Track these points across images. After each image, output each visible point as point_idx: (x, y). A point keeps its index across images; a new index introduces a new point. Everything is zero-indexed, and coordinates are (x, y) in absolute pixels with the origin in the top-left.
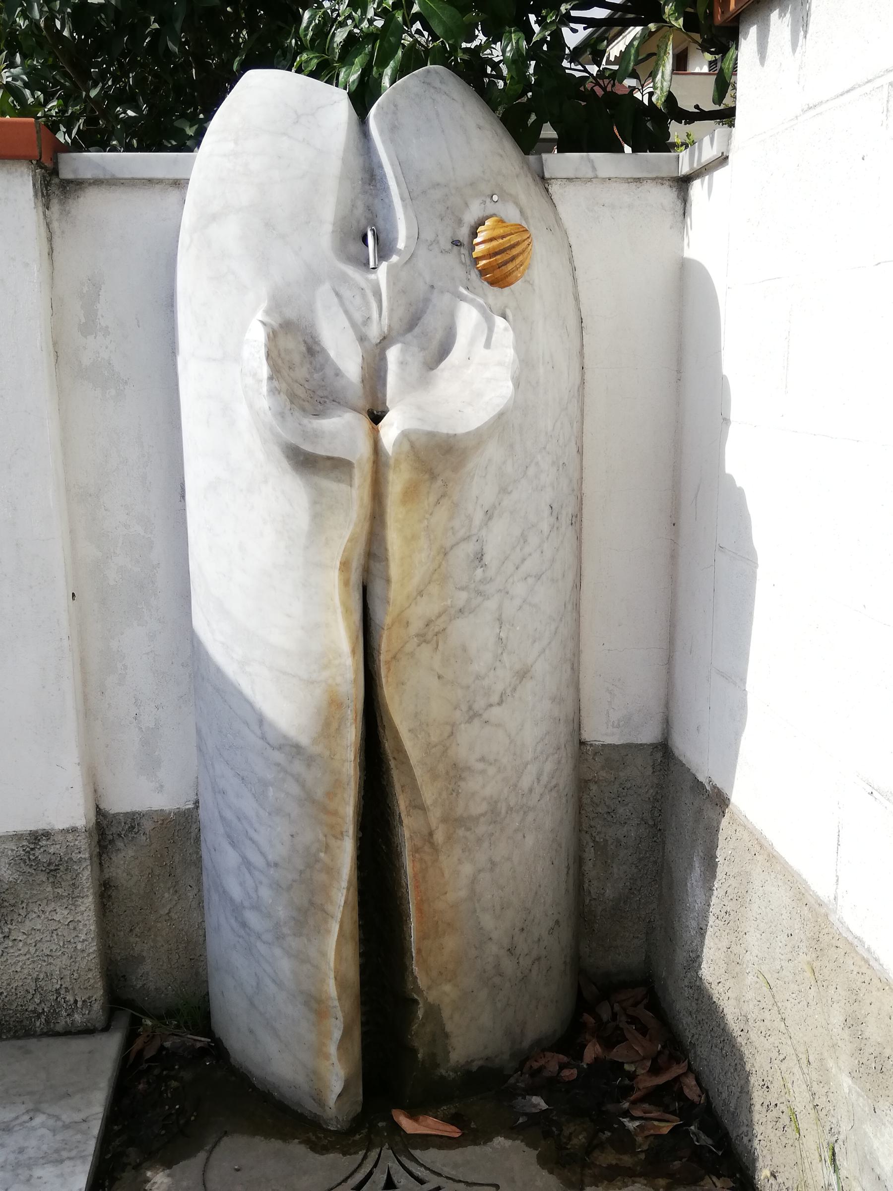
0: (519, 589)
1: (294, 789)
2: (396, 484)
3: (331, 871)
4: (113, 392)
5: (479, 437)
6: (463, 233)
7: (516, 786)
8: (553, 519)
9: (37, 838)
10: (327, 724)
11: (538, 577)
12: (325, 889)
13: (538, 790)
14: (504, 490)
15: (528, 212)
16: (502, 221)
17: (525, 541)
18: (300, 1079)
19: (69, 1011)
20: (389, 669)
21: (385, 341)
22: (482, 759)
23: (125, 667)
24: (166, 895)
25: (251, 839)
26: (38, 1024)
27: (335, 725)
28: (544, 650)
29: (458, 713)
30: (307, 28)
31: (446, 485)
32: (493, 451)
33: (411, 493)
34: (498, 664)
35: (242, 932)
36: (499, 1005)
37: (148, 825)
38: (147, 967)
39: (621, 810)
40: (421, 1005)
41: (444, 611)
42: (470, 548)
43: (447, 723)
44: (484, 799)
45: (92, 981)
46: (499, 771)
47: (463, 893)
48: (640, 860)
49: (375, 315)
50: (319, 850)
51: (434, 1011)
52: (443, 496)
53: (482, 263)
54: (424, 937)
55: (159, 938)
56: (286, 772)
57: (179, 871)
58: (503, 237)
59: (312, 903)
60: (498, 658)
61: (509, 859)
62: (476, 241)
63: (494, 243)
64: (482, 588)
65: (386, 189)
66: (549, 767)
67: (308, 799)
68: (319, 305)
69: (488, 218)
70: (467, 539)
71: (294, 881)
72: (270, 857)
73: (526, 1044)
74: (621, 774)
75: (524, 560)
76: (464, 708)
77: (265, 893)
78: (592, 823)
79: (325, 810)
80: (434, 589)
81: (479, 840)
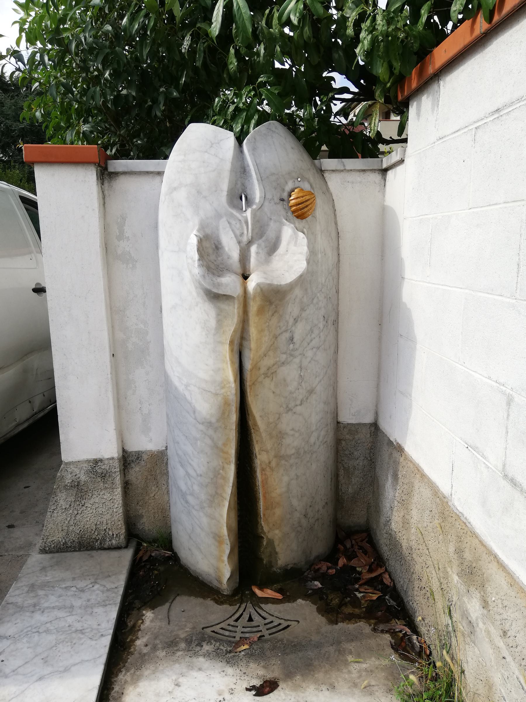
0: (310, 354)
1: (208, 441)
2: (253, 308)
3: (224, 478)
4: (131, 265)
5: (292, 286)
6: (285, 195)
7: (308, 442)
9: (97, 462)
10: (223, 413)
14: (303, 309)
15: (314, 186)
16: (302, 190)
18: (211, 571)
21: (250, 243)
22: (293, 429)
24: (153, 488)
25: (190, 464)
26: (97, 544)
28: (320, 381)
29: (282, 409)
30: (217, 106)
31: (276, 307)
32: (298, 292)
33: (261, 311)
34: (300, 387)
37: (145, 457)
38: (144, 520)
39: (356, 453)
42: (287, 335)
45: (120, 526)
49: (245, 232)
51: (271, 542)
52: (275, 312)
54: (266, 508)
58: (302, 197)
59: (217, 493)
60: (300, 384)
64: (292, 353)
65: (251, 176)
66: (323, 433)
67: (215, 446)
69: (296, 188)
70: (286, 331)
74: (356, 437)
75: (311, 340)
76: (285, 406)
80: (271, 353)
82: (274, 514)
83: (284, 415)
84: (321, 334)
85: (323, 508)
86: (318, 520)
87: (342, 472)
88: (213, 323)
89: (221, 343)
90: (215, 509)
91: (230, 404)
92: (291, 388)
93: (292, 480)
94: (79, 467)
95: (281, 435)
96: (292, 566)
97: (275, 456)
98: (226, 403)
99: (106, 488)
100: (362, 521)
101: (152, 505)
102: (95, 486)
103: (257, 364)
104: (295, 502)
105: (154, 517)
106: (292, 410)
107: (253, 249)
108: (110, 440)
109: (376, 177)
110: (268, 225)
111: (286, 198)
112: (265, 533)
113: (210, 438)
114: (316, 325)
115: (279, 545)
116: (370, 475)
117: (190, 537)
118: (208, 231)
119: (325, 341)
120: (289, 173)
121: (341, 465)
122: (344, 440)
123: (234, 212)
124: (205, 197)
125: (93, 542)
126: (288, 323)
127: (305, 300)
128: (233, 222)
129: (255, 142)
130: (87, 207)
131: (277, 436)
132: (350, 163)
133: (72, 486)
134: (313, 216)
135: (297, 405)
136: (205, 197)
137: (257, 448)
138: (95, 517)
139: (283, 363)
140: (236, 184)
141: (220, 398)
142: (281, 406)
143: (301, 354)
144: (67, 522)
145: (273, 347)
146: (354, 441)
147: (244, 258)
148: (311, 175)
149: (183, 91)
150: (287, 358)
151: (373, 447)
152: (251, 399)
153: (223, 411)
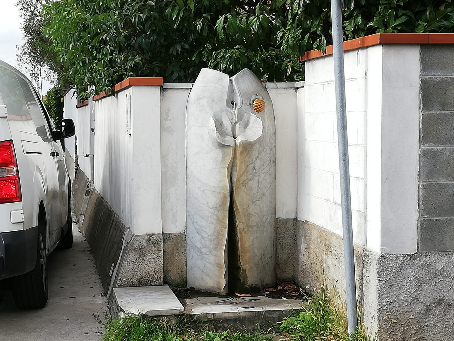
0: (263, 176)
1: (215, 217)
2: (239, 151)
3: (223, 236)
4: (171, 133)
5: (256, 142)
6: (251, 102)
7: (262, 220)
8: (269, 161)
9: (151, 235)
10: (223, 202)
11: (267, 173)
12: (222, 239)
13: (267, 222)
14: (259, 154)
15: (264, 97)
16: (259, 100)
17: (264, 165)
18: (215, 285)
19: (156, 280)
20: (236, 191)
21: (236, 123)
22: (255, 213)
23: (170, 197)
24: (177, 254)
25: (204, 231)
26: (148, 283)
27: (225, 203)
28: (268, 190)
29: (250, 202)
30: (214, 56)
31: (248, 151)
32: (257, 145)
33: (242, 153)
34: (258, 192)
35: (201, 255)
36: (259, 272)
37: (173, 237)
38: (171, 273)
39: (286, 236)
40: (241, 269)
41: (247, 179)
42: (253, 165)
43: (247, 204)
44: (255, 222)
45: (161, 272)
46: (258, 216)
47: (251, 243)
48: (291, 248)
49: (234, 118)
50: (220, 231)
51: (244, 271)
52: (248, 154)
53: (255, 108)
54: (242, 252)
55: (174, 266)
56: (213, 214)
57: (180, 248)
58: (259, 103)
59: (219, 243)
60: (258, 190)
61: (261, 237)
62: (254, 104)
63: (257, 104)
64: (255, 174)
65: (236, 94)
66: (269, 218)
67: (218, 220)
68: (223, 116)
69: (256, 99)
70: (252, 163)
71: (215, 238)
72: (209, 234)
73: (265, 284)
74: (286, 226)
75: (263, 169)
76: (251, 201)
77: (207, 243)
78: (279, 239)
79: (222, 222)
80: (245, 174)
81: (254, 231)
82: (246, 256)
83: (251, 205)
84: (268, 166)
85: (270, 258)
86: (267, 264)
87: (279, 247)
88: (220, 158)
89: (224, 168)
90: (218, 251)
91: (226, 198)
92: (254, 192)
93: (254, 239)
94: (142, 238)
95: (249, 215)
96: (255, 285)
97: (247, 226)
98: (225, 197)
99: (155, 250)
100: (290, 276)
101: (175, 264)
102: (150, 249)
103: (239, 178)
104: (256, 251)
105: (177, 271)
106: (254, 203)
107: (238, 125)
108: (159, 224)
109: (293, 91)
110: (244, 115)
111: (252, 104)
112: (241, 266)
113: (216, 215)
114: (265, 162)
115: (248, 273)
116: (294, 248)
117: (202, 271)
118: (217, 118)
119: (270, 170)
120: (253, 93)
121: (278, 242)
122: (280, 228)
123: (229, 109)
124: (216, 103)
125: (146, 281)
126: (253, 160)
127: (260, 149)
128: (229, 114)
129: (238, 80)
130: (155, 106)
131: (247, 215)
132: (280, 84)
133: (138, 249)
134: (263, 111)
135: (257, 201)
136: (216, 103)
137: (238, 222)
138: (148, 267)
139: (250, 179)
140: (230, 97)
141: (221, 195)
142: (249, 200)
143: (258, 175)
144: (134, 269)
145: (246, 171)
146: (285, 228)
147: (233, 130)
148: (262, 92)
149: (191, 44)
150: (252, 177)
151: (295, 232)
152: (235, 196)
153: (223, 201)
